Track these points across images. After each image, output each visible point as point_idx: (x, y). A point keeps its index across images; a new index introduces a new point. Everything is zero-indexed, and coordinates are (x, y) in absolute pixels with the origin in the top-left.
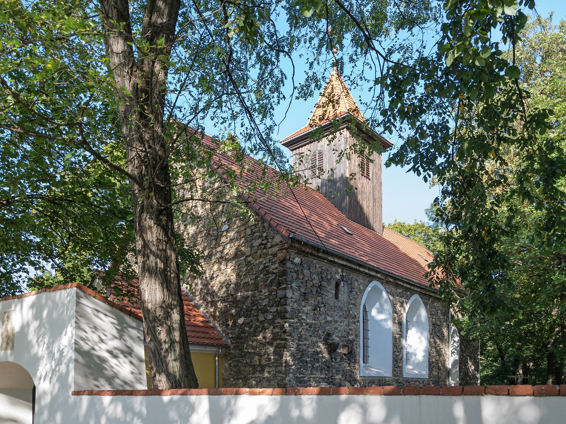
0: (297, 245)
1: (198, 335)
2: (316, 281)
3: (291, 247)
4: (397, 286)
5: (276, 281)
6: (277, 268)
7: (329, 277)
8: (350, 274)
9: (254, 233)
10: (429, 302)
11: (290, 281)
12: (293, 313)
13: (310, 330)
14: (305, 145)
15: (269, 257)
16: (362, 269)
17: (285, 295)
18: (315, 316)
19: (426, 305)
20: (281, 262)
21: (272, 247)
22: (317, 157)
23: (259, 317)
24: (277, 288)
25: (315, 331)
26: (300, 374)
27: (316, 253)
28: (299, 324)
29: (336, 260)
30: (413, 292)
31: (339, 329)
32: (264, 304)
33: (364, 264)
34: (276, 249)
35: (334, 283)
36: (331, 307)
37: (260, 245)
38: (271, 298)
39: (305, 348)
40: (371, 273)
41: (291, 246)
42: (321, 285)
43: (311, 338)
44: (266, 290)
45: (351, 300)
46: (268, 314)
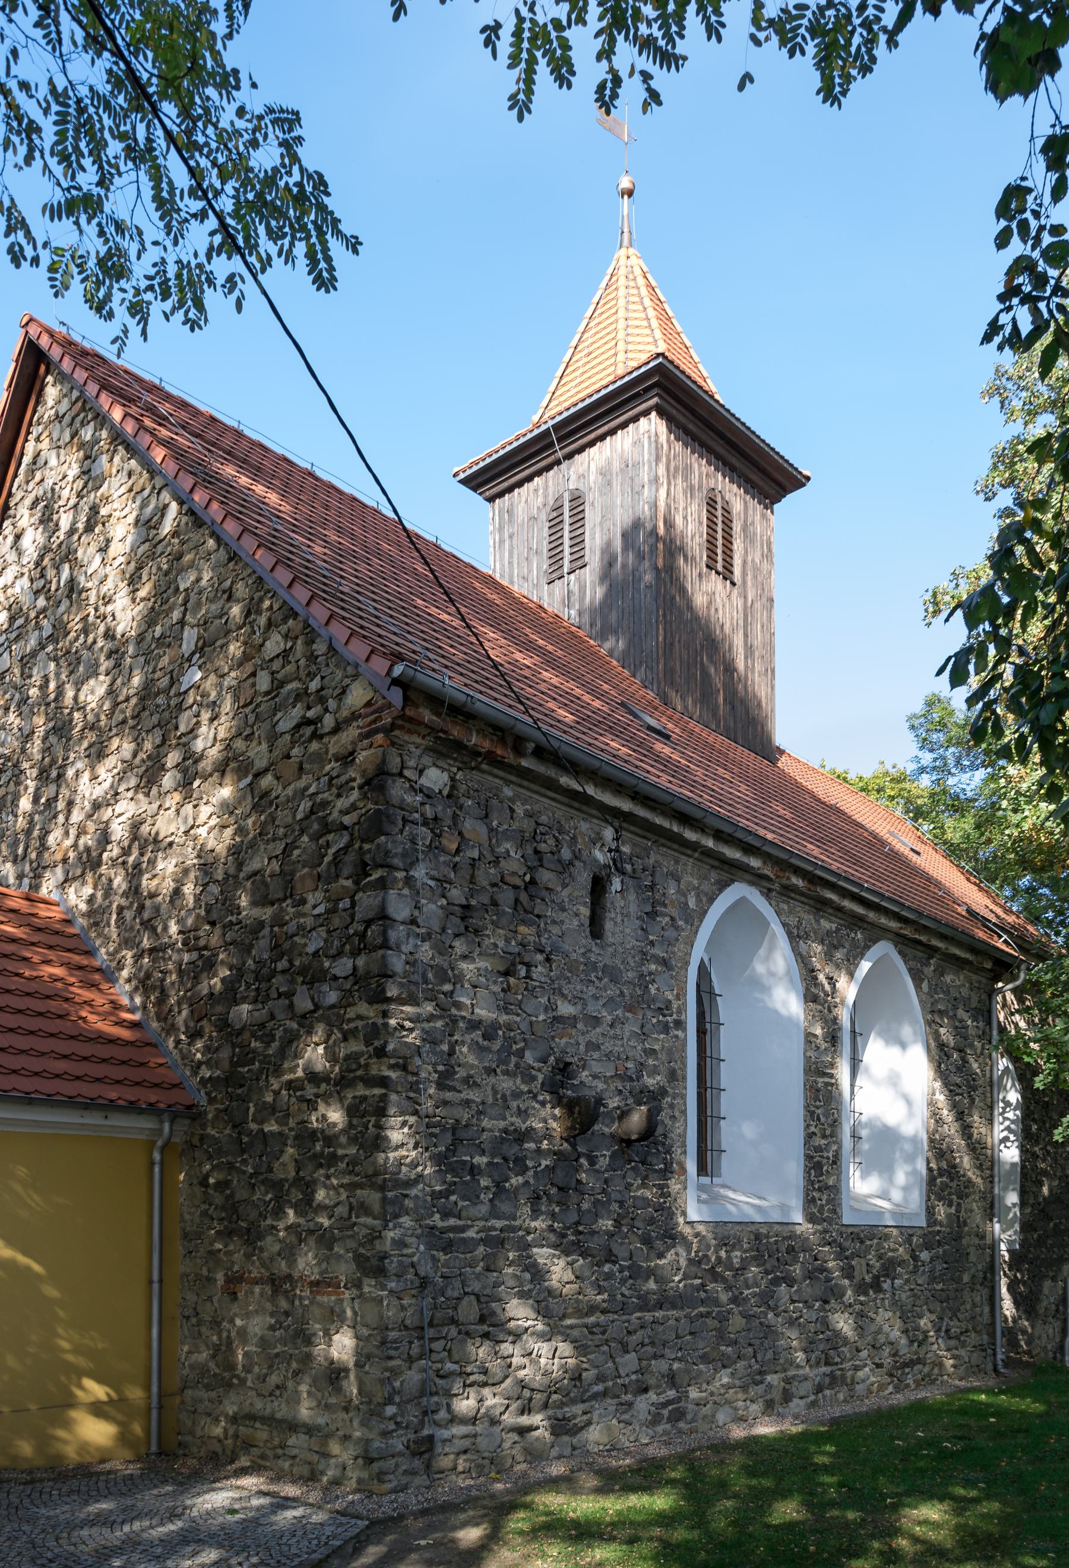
0: (427, 715)
1: (60, 1066)
2: (514, 864)
3: (405, 721)
4: (821, 906)
5: (351, 857)
6: (353, 807)
7: (566, 854)
8: (647, 850)
9: (282, 684)
10: (929, 970)
11: (404, 855)
12: (417, 978)
13: (488, 1050)
14: (529, 479)
15: (328, 768)
16: (690, 835)
17: (383, 907)
18: (510, 997)
19: (917, 977)
20: (368, 782)
21: (336, 730)
22: (567, 514)
23: (296, 999)
24: (357, 883)
25: (506, 1051)
26: (446, 1215)
27: (511, 758)
28: (439, 1024)
29: (590, 790)
30: (875, 934)
31: (607, 1046)
32: (311, 949)
33: (698, 815)
34: (352, 733)
35: (584, 878)
36: (572, 967)
37: (298, 726)
38: (336, 922)
39: (465, 1116)
40: (729, 852)
41: (402, 716)
42: (533, 882)
43: (492, 1080)
44: (319, 895)
45: (652, 943)
46: (325, 987)
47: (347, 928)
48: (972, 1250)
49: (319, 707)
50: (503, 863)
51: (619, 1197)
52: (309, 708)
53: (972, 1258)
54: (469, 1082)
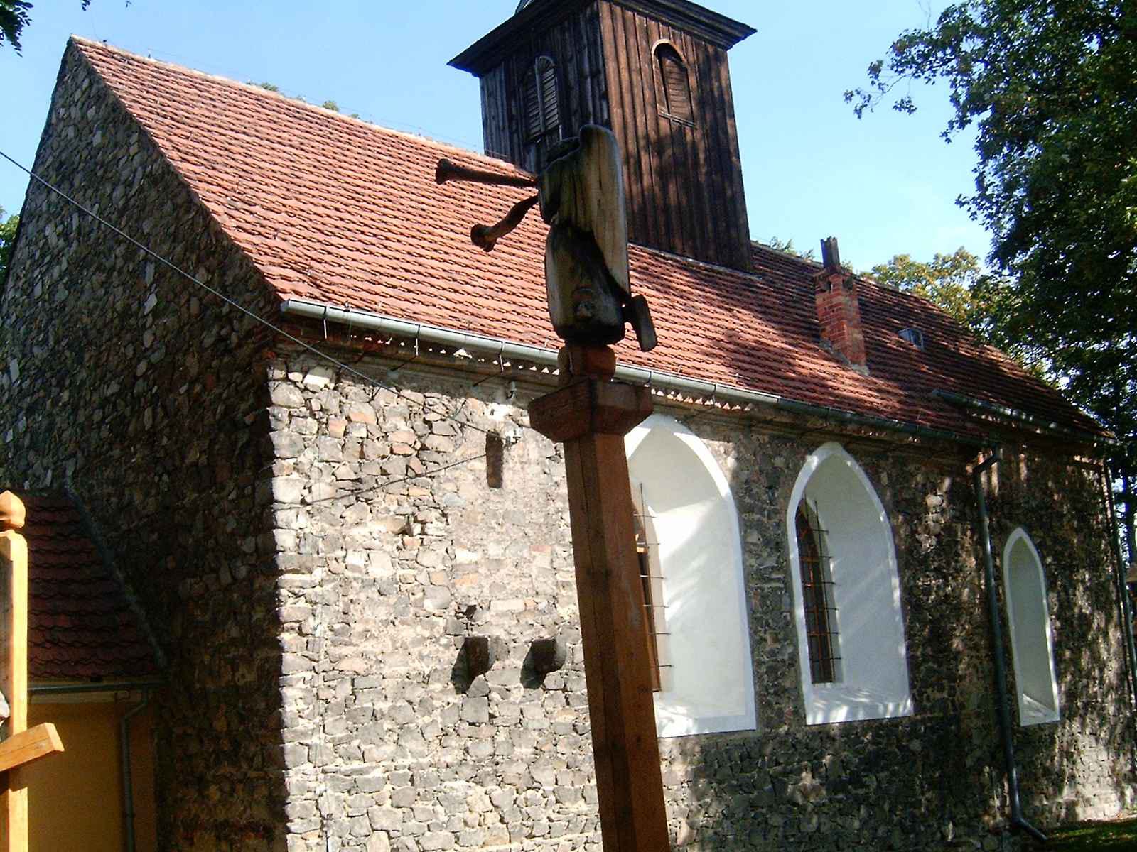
21: (239, 346)
42: (424, 448)
47: (250, 511)
48: (974, 733)
49: (228, 327)
50: (391, 436)
51: (537, 726)
52: (222, 328)
53: (976, 741)
54: (366, 635)
